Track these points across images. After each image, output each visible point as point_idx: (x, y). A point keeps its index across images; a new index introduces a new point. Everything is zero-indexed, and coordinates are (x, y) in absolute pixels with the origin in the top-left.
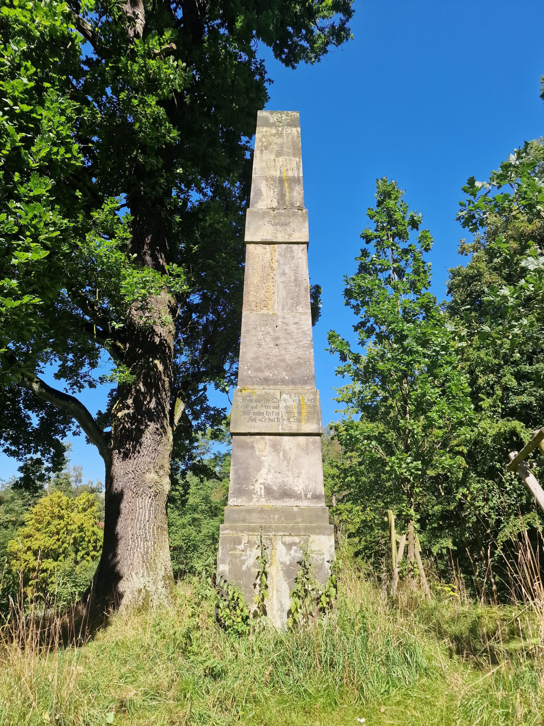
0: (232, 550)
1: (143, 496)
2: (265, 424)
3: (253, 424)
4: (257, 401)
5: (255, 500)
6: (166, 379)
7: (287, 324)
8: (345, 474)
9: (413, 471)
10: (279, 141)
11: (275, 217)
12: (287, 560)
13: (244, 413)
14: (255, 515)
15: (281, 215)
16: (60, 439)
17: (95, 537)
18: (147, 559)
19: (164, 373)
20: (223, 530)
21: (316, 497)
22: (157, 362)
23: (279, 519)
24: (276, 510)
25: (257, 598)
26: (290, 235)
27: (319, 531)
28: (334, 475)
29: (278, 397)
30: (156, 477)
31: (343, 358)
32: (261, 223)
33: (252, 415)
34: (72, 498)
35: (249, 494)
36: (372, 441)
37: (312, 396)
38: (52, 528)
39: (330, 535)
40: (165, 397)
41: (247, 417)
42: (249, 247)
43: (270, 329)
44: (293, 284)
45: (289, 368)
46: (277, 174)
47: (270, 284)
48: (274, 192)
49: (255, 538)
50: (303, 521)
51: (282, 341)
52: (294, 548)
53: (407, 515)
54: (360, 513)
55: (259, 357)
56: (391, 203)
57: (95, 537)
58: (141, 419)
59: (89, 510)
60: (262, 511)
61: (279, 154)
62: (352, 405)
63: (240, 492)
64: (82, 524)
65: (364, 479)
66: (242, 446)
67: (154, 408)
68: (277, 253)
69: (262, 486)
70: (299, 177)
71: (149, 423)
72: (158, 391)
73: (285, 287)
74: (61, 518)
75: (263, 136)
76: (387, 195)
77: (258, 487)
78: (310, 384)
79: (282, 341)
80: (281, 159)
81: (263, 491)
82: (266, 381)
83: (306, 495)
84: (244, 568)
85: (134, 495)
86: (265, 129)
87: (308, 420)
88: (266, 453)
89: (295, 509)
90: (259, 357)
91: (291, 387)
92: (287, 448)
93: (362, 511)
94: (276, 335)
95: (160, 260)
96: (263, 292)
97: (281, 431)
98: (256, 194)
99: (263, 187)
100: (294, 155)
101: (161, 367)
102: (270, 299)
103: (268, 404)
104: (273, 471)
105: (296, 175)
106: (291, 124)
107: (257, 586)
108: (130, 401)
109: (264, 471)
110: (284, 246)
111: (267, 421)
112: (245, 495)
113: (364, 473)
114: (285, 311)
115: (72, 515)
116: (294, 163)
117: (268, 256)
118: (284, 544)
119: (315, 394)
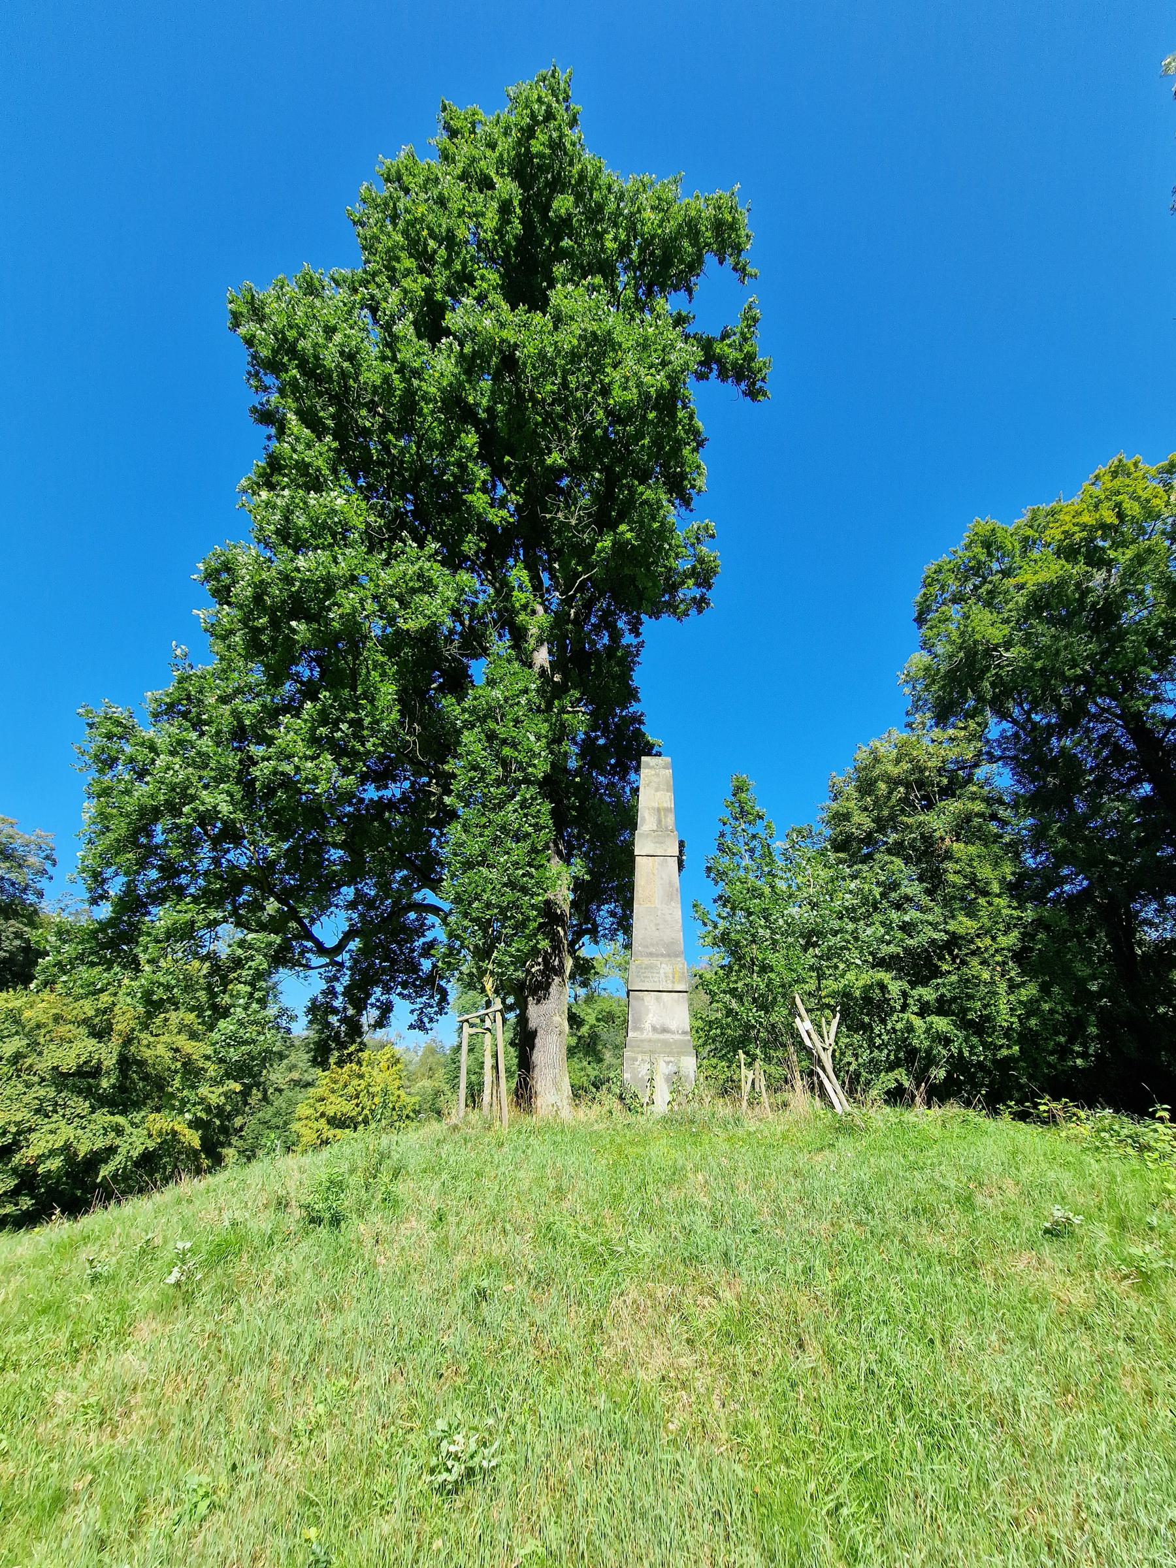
21: (684, 1033)
22: (559, 929)
25: (648, 1093)
27: (687, 1054)
31: (705, 924)
35: (641, 1030)
38: (350, 1090)
46: (656, 805)
51: (661, 927)
60: (650, 1041)
61: (657, 790)
63: (636, 1029)
66: (637, 998)
72: (560, 951)
74: (361, 1076)
76: (738, 790)
77: (647, 1026)
79: (661, 927)
82: (651, 954)
99: (647, 815)
101: (562, 933)
109: (651, 1015)
115: (374, 1073)
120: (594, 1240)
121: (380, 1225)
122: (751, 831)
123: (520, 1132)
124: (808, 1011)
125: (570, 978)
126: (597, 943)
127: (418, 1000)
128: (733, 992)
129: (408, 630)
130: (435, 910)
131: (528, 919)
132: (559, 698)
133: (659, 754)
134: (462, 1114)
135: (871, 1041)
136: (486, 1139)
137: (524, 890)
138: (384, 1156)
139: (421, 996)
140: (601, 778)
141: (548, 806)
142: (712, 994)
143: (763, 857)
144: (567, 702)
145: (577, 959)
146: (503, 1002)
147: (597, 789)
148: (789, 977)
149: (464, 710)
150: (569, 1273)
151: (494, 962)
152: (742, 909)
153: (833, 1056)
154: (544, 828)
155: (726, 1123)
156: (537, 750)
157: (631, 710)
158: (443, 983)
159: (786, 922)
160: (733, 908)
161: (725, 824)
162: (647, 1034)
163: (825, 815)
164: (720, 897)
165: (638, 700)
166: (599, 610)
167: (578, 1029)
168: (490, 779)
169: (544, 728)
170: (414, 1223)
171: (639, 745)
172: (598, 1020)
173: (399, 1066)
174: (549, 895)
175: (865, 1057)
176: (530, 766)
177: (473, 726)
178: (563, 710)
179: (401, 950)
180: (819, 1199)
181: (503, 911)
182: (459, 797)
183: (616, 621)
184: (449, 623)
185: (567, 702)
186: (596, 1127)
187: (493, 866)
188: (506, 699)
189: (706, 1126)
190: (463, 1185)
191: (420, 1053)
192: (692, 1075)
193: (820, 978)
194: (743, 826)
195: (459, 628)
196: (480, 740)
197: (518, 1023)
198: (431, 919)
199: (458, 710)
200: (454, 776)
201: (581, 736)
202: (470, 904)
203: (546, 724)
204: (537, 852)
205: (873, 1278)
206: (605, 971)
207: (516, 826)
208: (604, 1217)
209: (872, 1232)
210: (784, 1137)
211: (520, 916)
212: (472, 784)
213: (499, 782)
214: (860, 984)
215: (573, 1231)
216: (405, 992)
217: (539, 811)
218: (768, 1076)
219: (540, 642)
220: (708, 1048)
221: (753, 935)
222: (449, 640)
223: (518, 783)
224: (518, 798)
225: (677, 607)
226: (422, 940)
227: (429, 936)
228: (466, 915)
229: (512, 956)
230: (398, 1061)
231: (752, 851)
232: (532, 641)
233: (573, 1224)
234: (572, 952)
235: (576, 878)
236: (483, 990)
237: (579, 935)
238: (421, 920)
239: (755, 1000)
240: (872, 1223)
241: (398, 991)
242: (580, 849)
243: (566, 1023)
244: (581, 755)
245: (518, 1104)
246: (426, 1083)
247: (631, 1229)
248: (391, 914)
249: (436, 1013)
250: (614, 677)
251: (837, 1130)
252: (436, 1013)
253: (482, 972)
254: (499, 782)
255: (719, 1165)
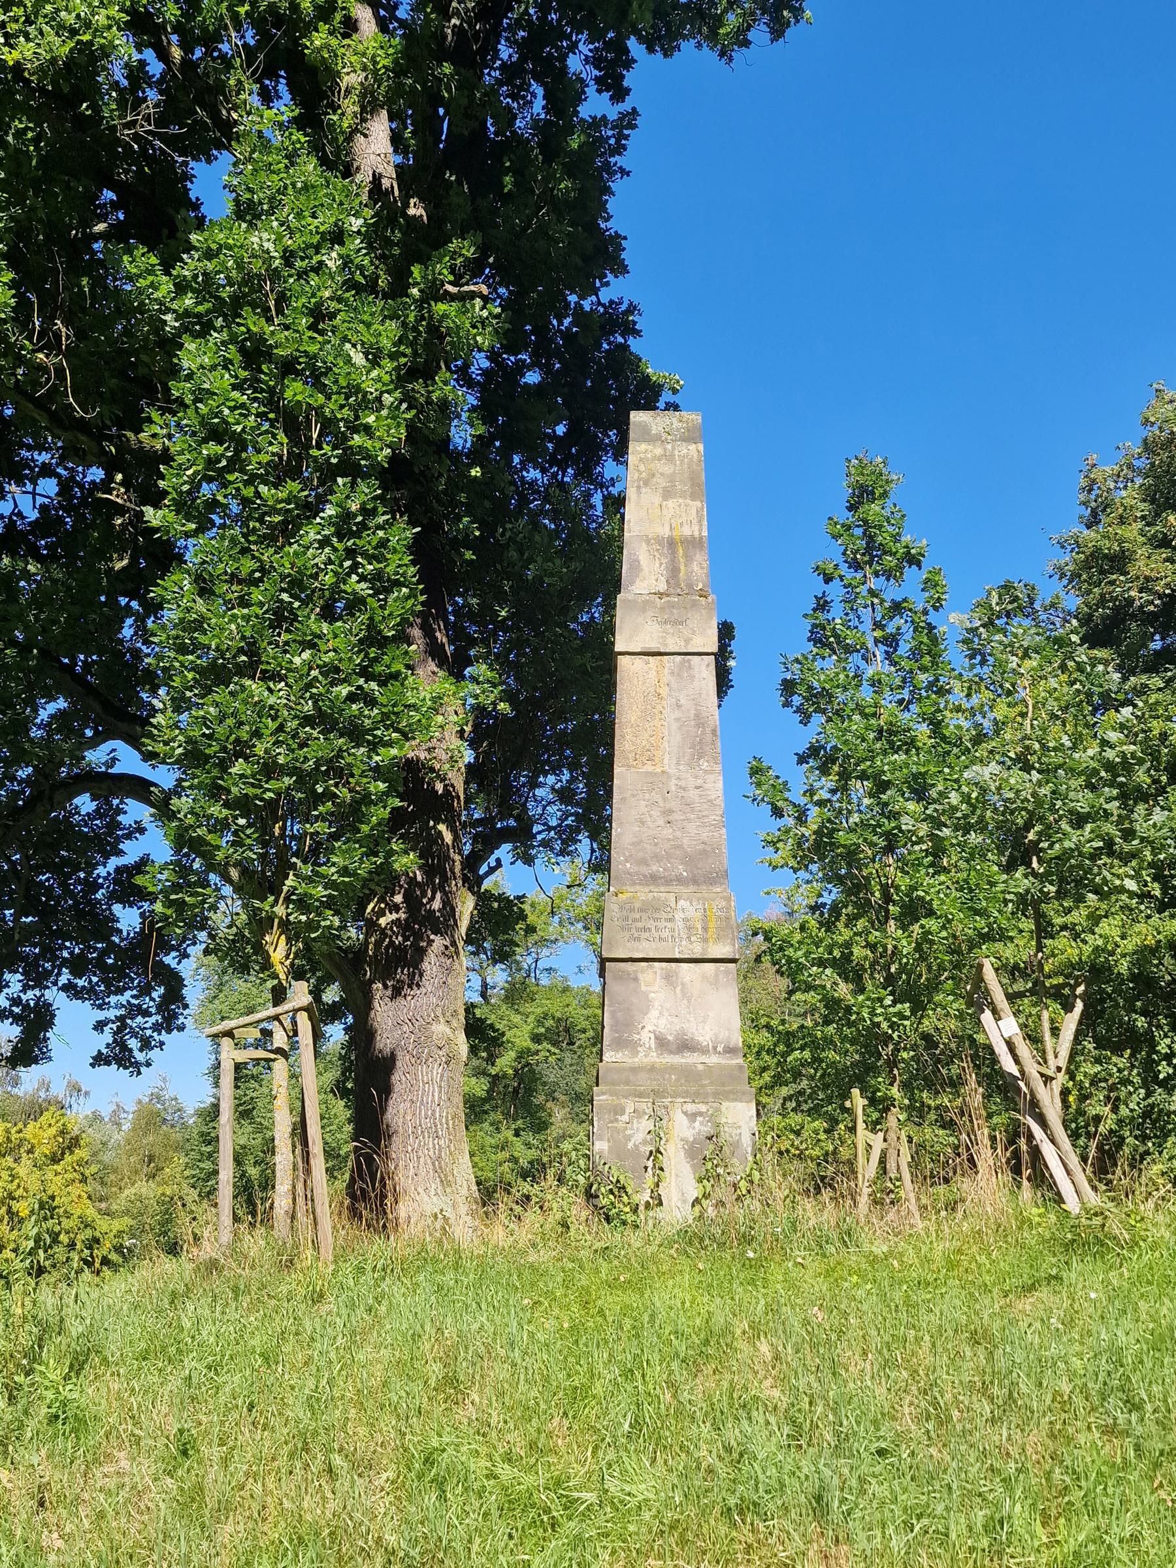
0: (612, 1122)
1: (429, 1063)
2: (654, 945)
3: (637, 944)
4: (641, 910)
5: (641, 1055)
6: (457, 858)
7: (684, 789)
8: (788, 1045)
9: (894, 1019)
10: (667, 469)
11: (662, 609)
12: (689, 1135)
13: (623, 929)
14: (643, 1076)
15: (672, 606)
16: (173, 964)
17: (89, 1232)
18: (441, 1168)
19: (454, 847)
20: (598, 1095)
22: (442, 827)
23: (677, 1080)
24: (672, 1068)
25: (650, 1180)
26: (687, 641)
27: (734, 1096)
28: (762, 1048)
29: (673, 905)
30: (448, 1030)
31: (778, 812)
32: (640, 620)
33: (634, 931)
34: (20, 1125)
35: (633, 1046)
36: (826, 967)
37: (724, 903)
39: (750, 1101)
40: (454, 889)
41: (627, 934)
42: (623, 661)
43: (656, 797)
44: (693, 723)
45: (689, 860)
46: (665, 532)
47: (657, 723)
48: (661, 564)
49: (644, 1106)
50: (711, 1083)
51: (677, 816)
52: (699, 1119)
53: (886, 1098)
54: (823, 1136)
55: (641, 841)
56: (873, 510)
57: (89, 1233)
58: (420, 929)
59: (68, 1158)
60: (652, 1069)
61: (667, 494)
62: (808, 876)
63: (620, 1044)
64: (53, 1198)
65: (831, 1055)
67: (439, 910)
68: (666, 671)
69: (652, 1036)
70: (701, 538)
71: (432, 937)
72: (445, 879)
73: (680, 728)
75: (641, 460)
77: (646, 1037)
78: (721, 884)
79: (677, 816)
80: (671, 503)
81: (653, 1041)
82: (654, 879)
83: (715, 1048)
84: (630, 1145)
85: (413, 1061)
86: (643, 446)
87: (718, 939)
88: (656, 988)
89: (700, 1067)
90: (641, 841)
91: (692, 888)
92: (687, 980)
93: (826, 1131)
94: (668, 806)
95: (438, 634)
96: (646, 735)
97: (677, 956)
98: (631, 568)
100: (693, 497)
101: (448, 837)
102: (658, 748)
103: (657, 915)
104: (666, 1014)
105: (696, 534)
106: (688, 439)
107: (649, 1170)
108: (398, 899)
109: (654, 1013)
110: (678, 658)
111: (657, 940)
112: (627, 1047)
113: (832, 1042)
114: (681, 767)
116: (694, 512)
117: (653, 674)
118: (685, 1113)
119: (728, 899)
120: (529, 1480)
121: (47, 1472)
122: (893, 592)
123: (360, 1270)
124: (1011, 997)
125: (469, 941)
126: (529, 861)
127: (113, 999)
128: (845, 967)
129: (18, 68)
130: (139, 788)
131: (365, 799)
132: (424, 260)
133: (673, 407)
134: (226, 1237)
135: (1149, 1068)
136: (284, 1289)
137: (356, 734)
138: (46, 1331)
139: (120, 991)
140: (533, 474)
141: (402, 533)
142: (792, 970)
143: (916, 654)
144: (442, 270)
145: (484, 899)
146: (316, 993)
147: (524, 501)
148: (965, 927)
149: (181, 288)
150: (475, 1548)
151: (287, 900)
152: (863, 776)
153: (1065, 1093)
154: (398, 584)
155: (821, 1243)
156: (371, 389)
157: (605, 295)
158: (170, 960)
159: (966, 799)
160: (845, 776)
161: (828, 579)
162: (648, 1055)
163: (1066, 559)
164: (814, 751)
165: (621, 269)
166: (518, 24)
167: (491, 1059)
168: (255, 461)
169: (388, 333)
170: (125, 1464)
171: (623, 391)
172: (536, 1038)
173: (79, 1153)
174: (413, 750)
175: (1135, 1103)
176: (355, 430)
177: (207, 328)
178: (433, 293)
179: (64, 885)
180: (1025, 1386)
181: (304, 779)
182: (183, 506)
183: (563, 58)
184: (125, 48)
185: (442, 270)
186: (532, 1257)
187: (276, 677)
188: (288, 257)
189: (779, 1247)
190: (233, 1381)
191: (126, 1127)
192: (747, 1141)
193: (1044, 930)
194: (873, 583)
195: (156, 68)
196: (226, 364)
197: (351, 1044)
198: (135, 811)
199: (166, 285)
200: (166, 457)
201: (481, 362)
202: (224, 766)
203: (392, 325)
204: (382, 643)
205: (1135, 1538)
206: (552, 929)
207: (329, 579)
208: (550, 1435)
209: (1137, 1448)
210: (951, 1265)
211: (344, 793)
212: (214, 472)
213: (281, 472)
214: (1129, 945)
215: (484, 1463)
216: (81, 983)
217: (383, 543)
218: (919, 1149)
219: (368, 107)
220: (785, 1091)
221: (888, 835)
222: (130, 98)
223: (328, 474)
224: (330, 511)
225: (719, 21)
226: (114, 862)
227: (132, 851)
228: (215, 792)
229: (329, 885)
230: (75, 1143)
231: (891, 641)
232: (350, 106)
233: (483, 1450)
234: (473, 882)
235: (480, 711)
236: (266, 965)
237: (488, 841)
238: (111, 815)
239: (890, 980)
240: (1139, 1430)
241: (63, 980)
242: (485, 642)
243: (462, 1037)
244: (485, 411)
245: (355, 1214)
246: (146, 1189)
247: (611, 1455)
248: (31, 803)
249: (157, 1028)
250: (558, 206)
251: (1068, 1246)
252: (157, 1028)
253: (261, 924)
254: (281, 472)
255: (806, 1322)
